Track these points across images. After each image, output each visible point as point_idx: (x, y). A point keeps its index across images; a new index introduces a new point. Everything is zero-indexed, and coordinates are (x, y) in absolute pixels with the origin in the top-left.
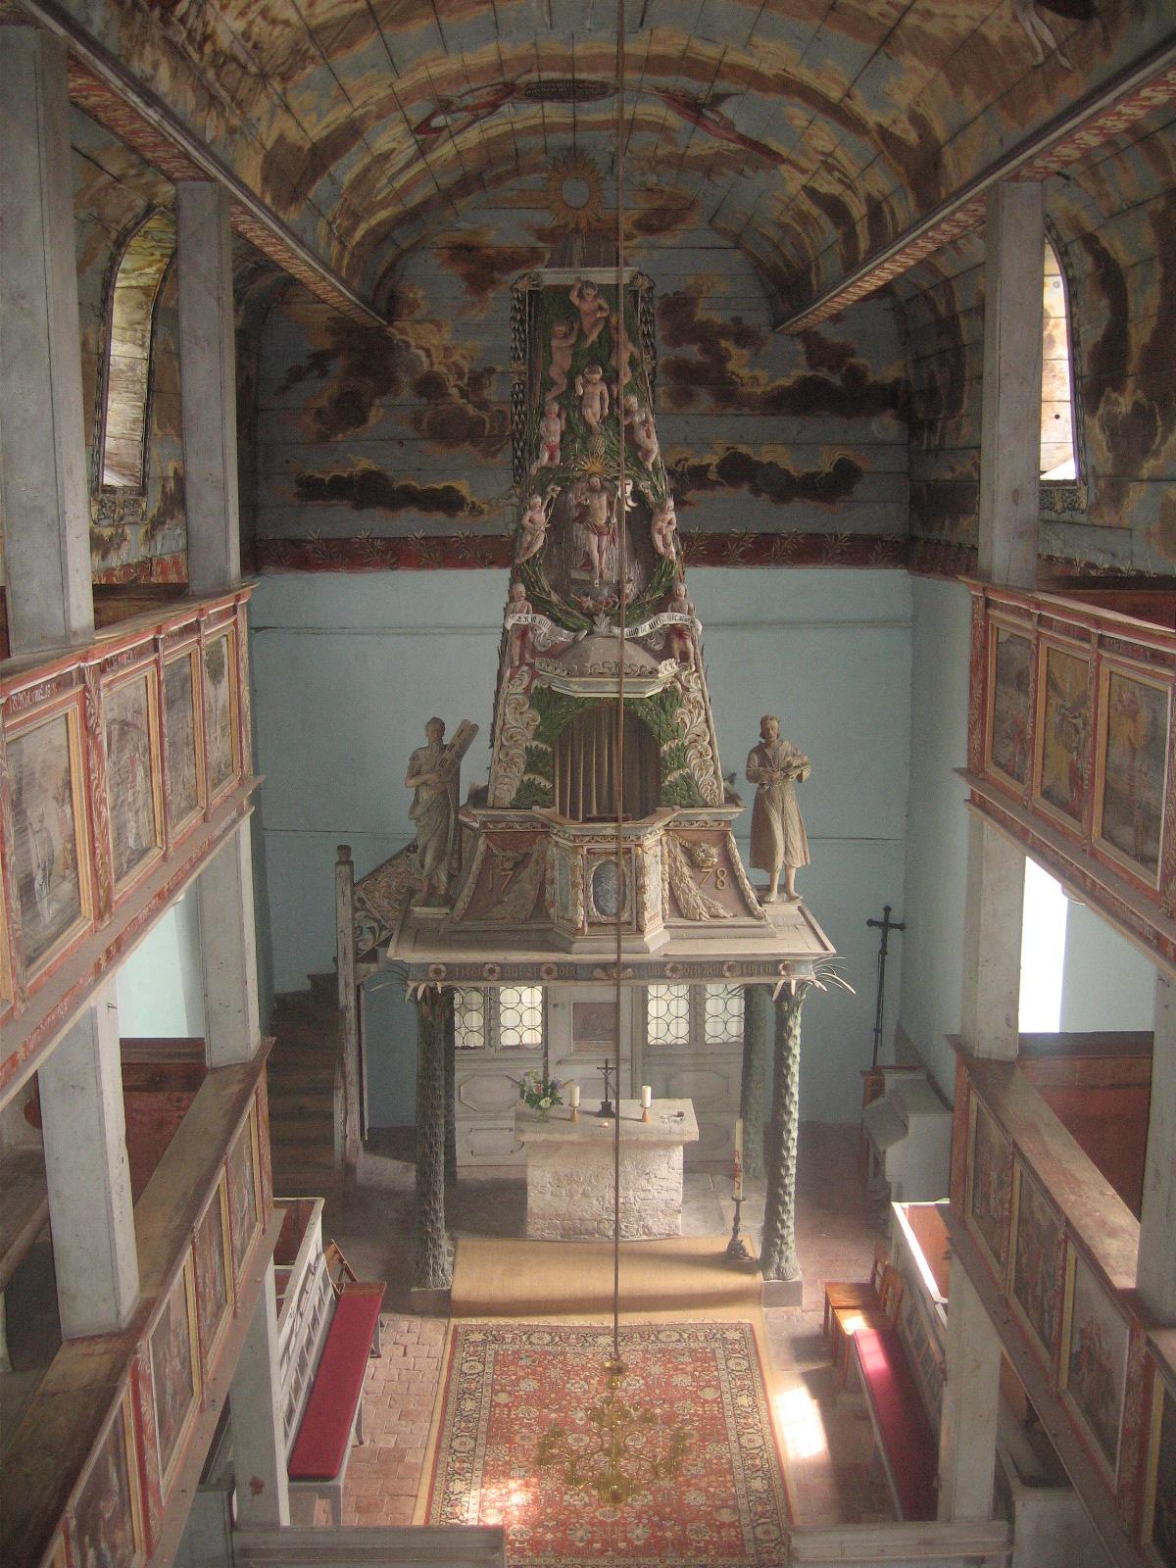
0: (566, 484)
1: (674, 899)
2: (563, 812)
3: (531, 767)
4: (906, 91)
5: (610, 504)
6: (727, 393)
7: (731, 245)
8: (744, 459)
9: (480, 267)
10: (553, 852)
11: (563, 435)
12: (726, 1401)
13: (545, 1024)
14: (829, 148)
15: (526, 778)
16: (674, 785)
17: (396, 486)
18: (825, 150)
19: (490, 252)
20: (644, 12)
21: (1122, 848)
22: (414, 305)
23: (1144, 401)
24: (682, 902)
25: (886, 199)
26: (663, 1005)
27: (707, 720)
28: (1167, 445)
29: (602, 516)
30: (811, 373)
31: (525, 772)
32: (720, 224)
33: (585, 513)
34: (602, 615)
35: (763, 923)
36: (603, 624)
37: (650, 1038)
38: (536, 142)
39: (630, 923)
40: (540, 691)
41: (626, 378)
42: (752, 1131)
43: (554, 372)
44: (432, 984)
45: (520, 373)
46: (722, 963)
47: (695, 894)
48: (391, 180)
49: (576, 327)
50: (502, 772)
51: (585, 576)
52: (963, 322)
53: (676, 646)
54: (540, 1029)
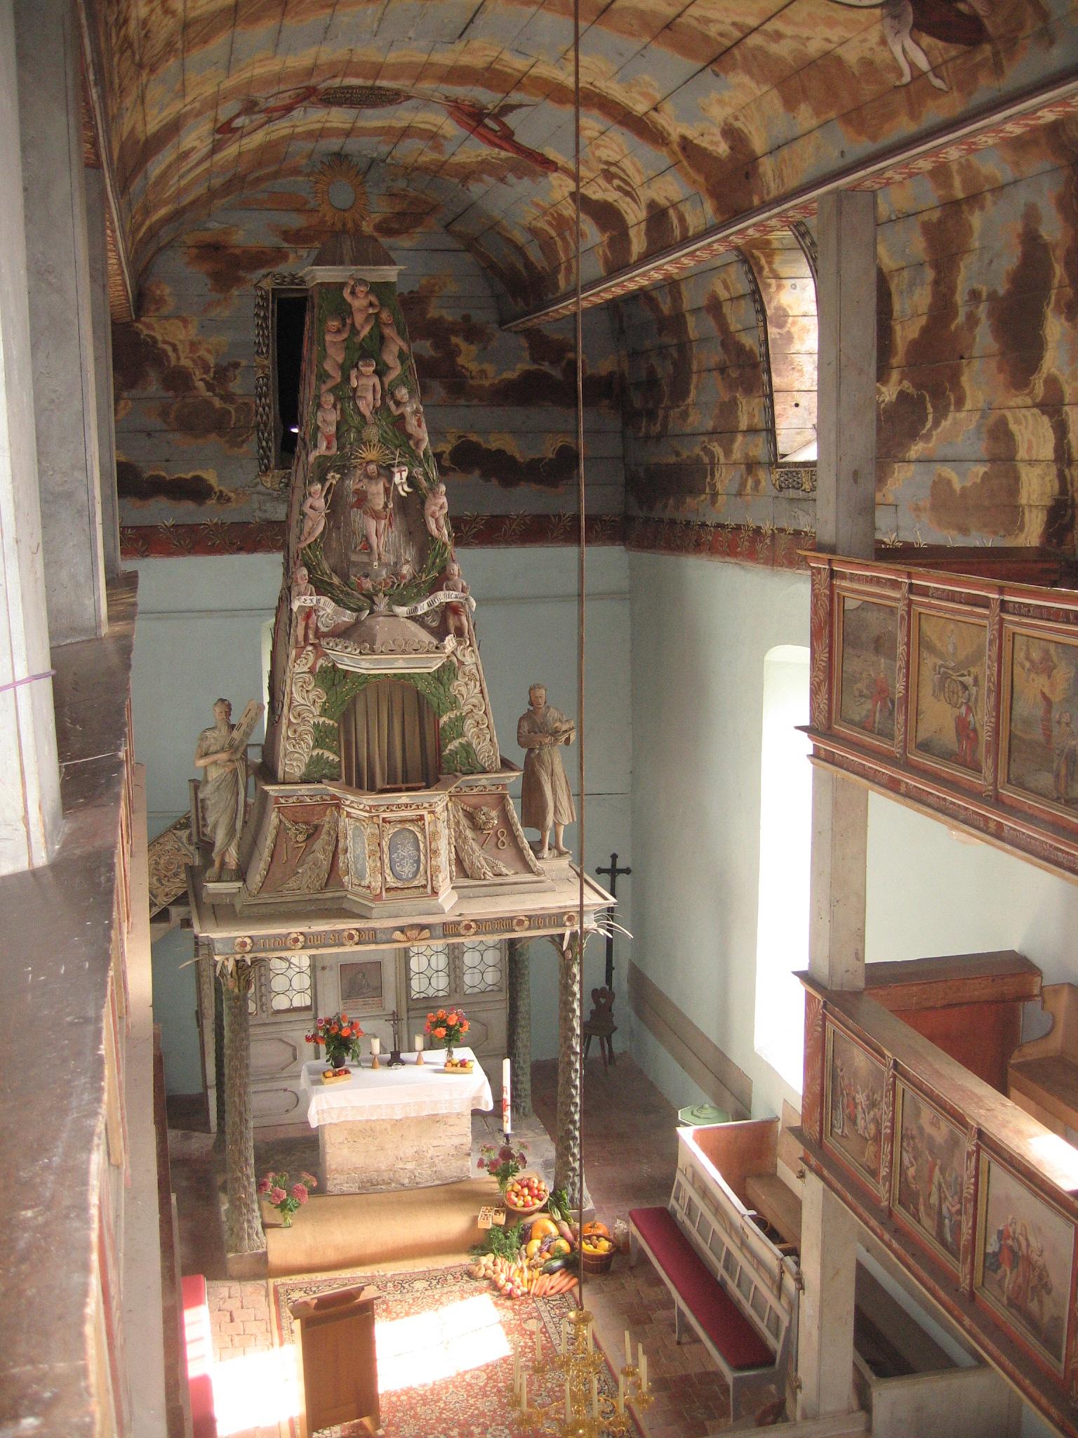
0: (344, 470)
1: (459, 862)
2: (349, 783)
3: (318, 743)
4: (718, 110)
5: (387, 490)
6: (458, 385)
7: (462, 248)
8: (475, 447)
9: (224, 264)
10: (344, 822)
11: (338, 424)
12: (551, 1331)
13: (314, 986)
14: (614, 157)
15: (315, 753)
16: (454, 753)
17: (146, 476)
18: (610, 160)
19: (237, 251)
20: (472, 21)
21: (1039, 794)
22: (160, 302)
23: (911, 390)
24: (466, 864)
25: (674, 205)
26: (424, 960)
27: (482, 692)
28: (939, 430)
29: (379, 502)
30: (535, 367)
31: (314, 748)
32: (457, 227)
33: (362, 499)
34: (381, 595)
35: (542, 878)
36: (382, 604)
37: (413, 993)
38: (308, 146)
39: (425, 887)
40: (324, 670)
41: (396, 372)
42: (520, 1072)
43: (328, 366)
44: (238, 957)
45: (263, 367)
46: (512, 918)
47: (478, 856)
48: (181, 177)
49: (348, 321)
50: (291, 749)
51: (365, 559)
52: (691, 321)
53: (452, 622)
54: (309, 992)
